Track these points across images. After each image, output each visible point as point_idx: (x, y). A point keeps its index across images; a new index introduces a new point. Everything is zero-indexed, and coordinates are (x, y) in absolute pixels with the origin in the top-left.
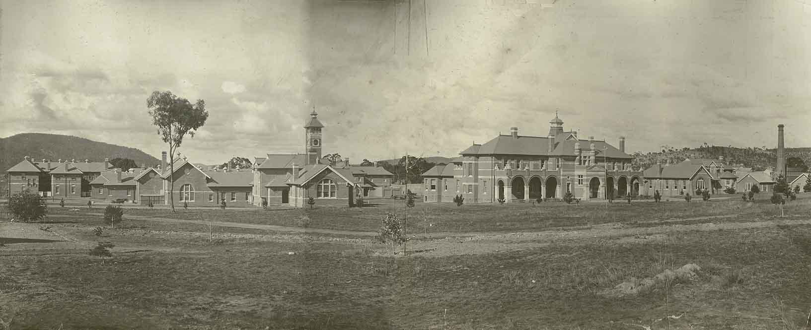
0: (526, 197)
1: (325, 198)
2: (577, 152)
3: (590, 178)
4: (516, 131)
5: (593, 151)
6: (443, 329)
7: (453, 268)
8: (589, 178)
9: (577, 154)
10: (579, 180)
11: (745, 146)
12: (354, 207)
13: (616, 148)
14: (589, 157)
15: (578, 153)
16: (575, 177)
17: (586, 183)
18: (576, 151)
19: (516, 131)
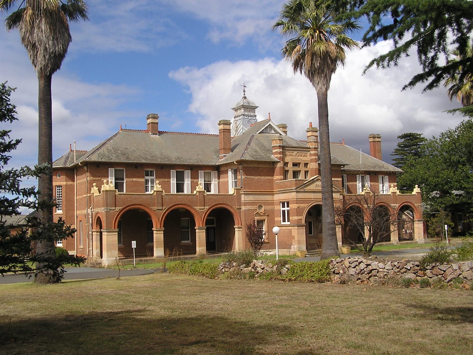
0: (158, 252)
1: (192, 194)
2: (276, 153)
3: (306, 207)
4: (227, 127)
5: (312, 152)
6: (472, 166)
7: (122, 292)
8: (303, 205)
9: (274, 157)
10: (284, 212)
11: (317, 95)
12: (50, 258)
13: (70, 251)
14: (306, 165)
15: (279, 156)
16: (276, 208)
17: (296, 218)
18: (187, 189)
19: (227, 127)
